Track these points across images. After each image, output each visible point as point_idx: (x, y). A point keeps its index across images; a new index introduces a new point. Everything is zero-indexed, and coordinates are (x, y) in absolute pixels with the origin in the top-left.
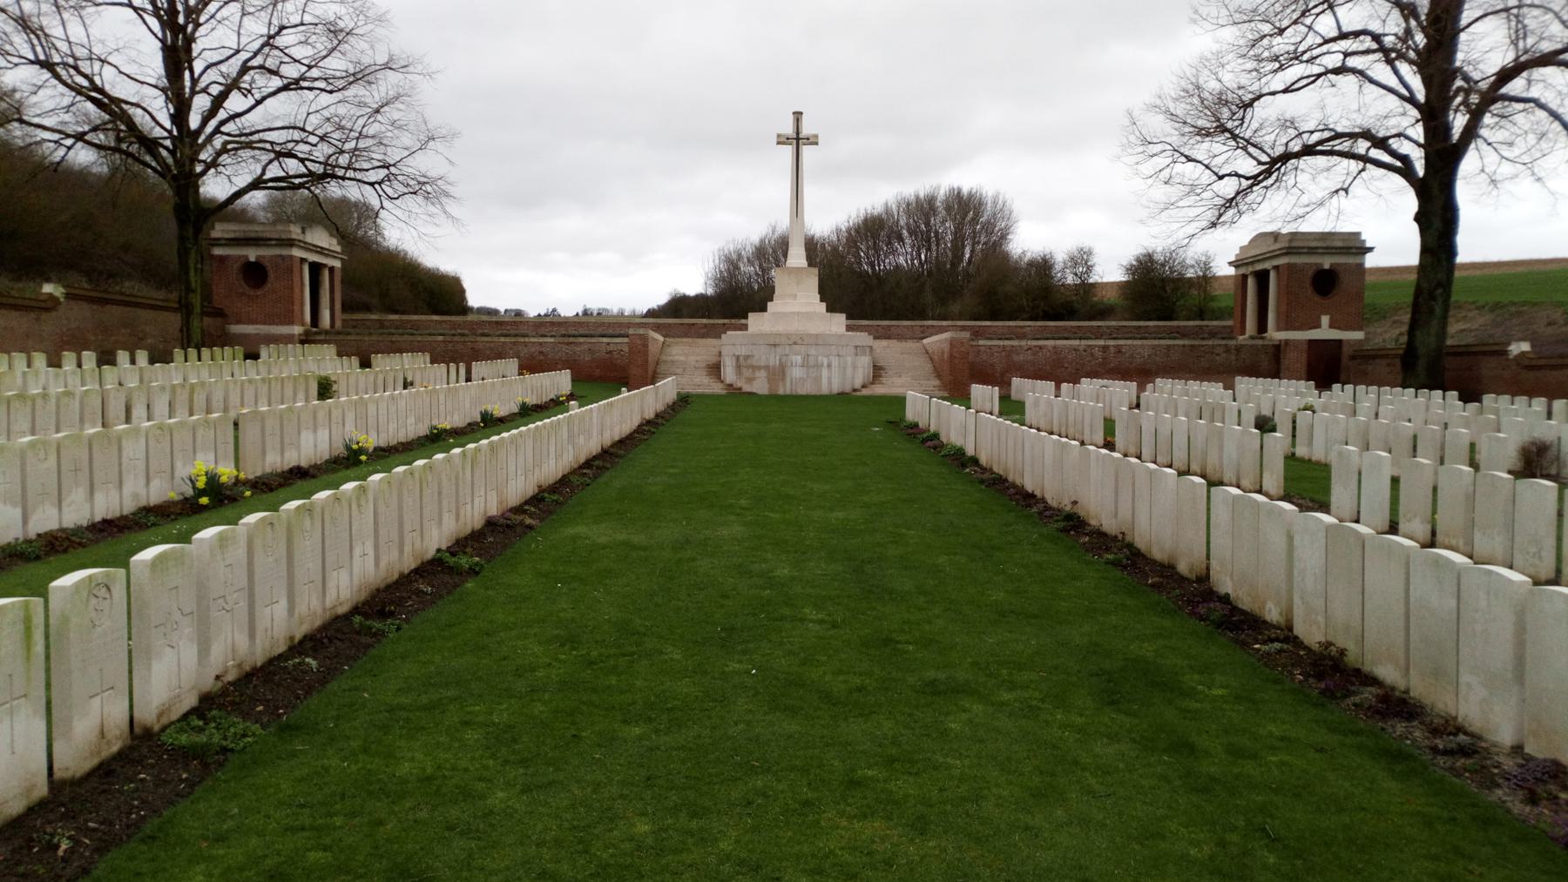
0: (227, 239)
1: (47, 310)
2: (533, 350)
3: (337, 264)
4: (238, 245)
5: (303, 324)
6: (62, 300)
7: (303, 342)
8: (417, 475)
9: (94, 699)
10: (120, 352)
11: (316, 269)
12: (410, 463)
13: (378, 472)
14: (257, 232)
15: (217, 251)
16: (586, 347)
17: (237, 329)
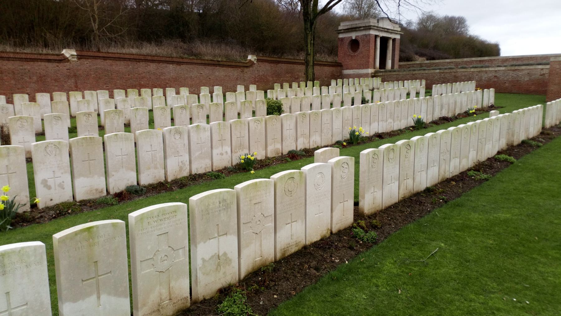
0: (344, 30)
1: (247, 67)
2: (490, 75)
3: (398, 37)
4: (347, 32)
5: (374, 68)
6: (255, 62)
7: (373, 77)
8: (477, 127)
9: (288, 225)
10: (239, 86)
11: (384, 41)
12: (435, 131)
13: (540, 104)
14: (356, 24)
15: (341, 36)
16: (526, 72)
17: (346, 72)
